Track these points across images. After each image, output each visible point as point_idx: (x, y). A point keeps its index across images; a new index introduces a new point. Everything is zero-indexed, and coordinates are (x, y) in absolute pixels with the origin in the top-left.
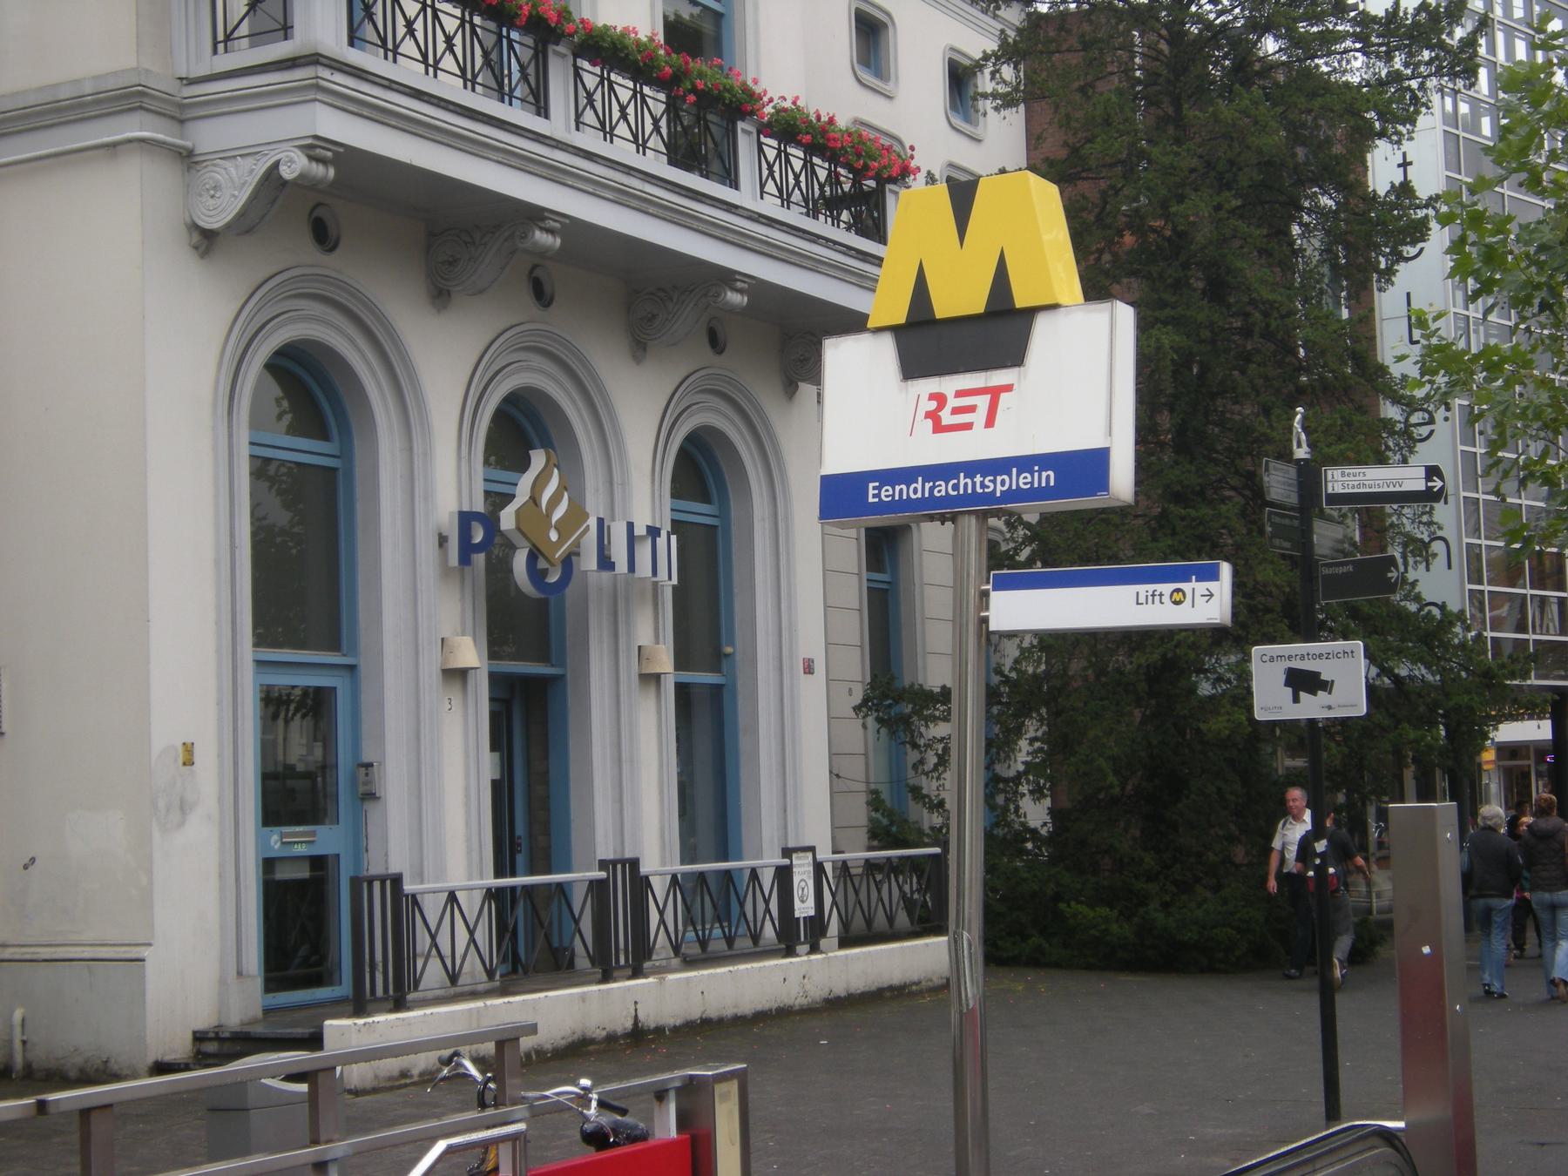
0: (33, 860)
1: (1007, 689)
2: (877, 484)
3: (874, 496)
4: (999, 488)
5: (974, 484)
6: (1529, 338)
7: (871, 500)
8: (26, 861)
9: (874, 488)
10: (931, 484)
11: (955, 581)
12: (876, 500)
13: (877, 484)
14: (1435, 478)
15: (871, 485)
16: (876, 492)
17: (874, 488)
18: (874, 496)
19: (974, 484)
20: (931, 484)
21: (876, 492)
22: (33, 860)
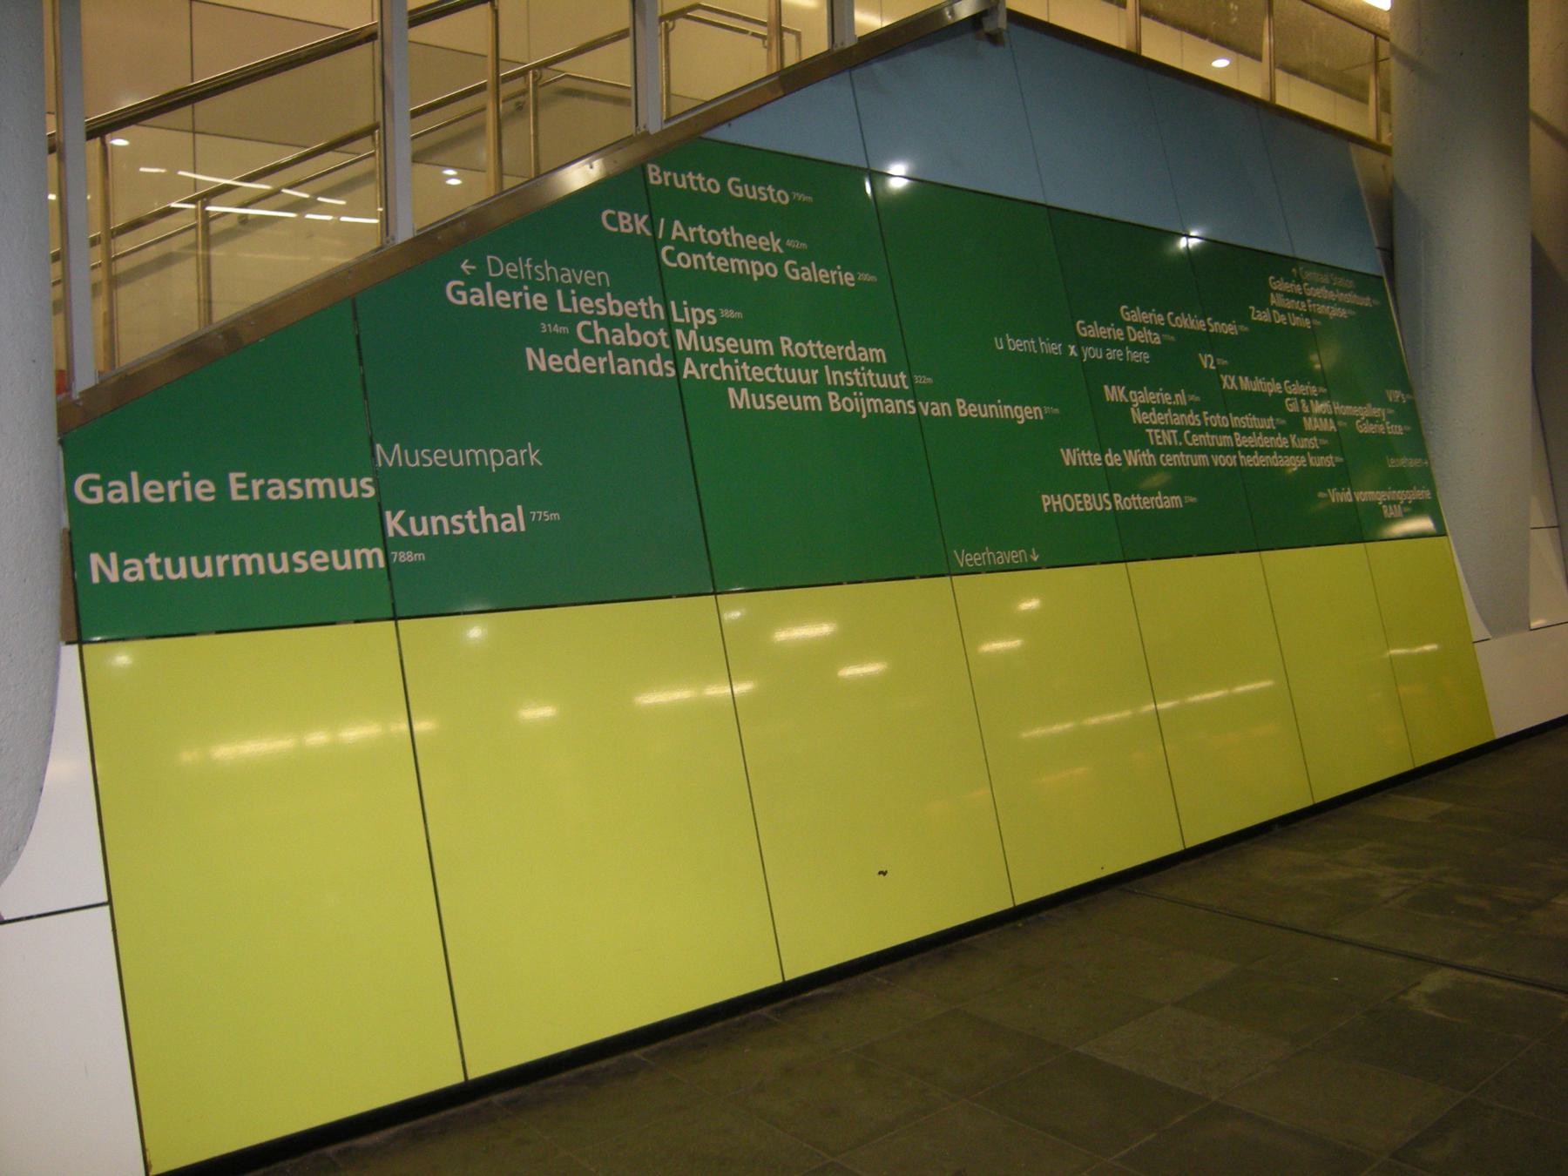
0: (880, 873)
1: (1236, 8)
2: (243, 475)
3: (240, 492)
4: (576, 359)
5: (147, 568)
6: (374, 140)
7: (235, 497)
8: (881, 875)
9: (239, 480)
10: (262, 482)
11: (185, 105)
12: (245, 497)
13: (243, 475)
14: (468, 273)
15: (233, 476)
16: (243, 486)
17: (239, 480)
18: (240, 492)
19: (147, 568)
20: (262, 482)
21: (243, 486)
22: (880, 873)
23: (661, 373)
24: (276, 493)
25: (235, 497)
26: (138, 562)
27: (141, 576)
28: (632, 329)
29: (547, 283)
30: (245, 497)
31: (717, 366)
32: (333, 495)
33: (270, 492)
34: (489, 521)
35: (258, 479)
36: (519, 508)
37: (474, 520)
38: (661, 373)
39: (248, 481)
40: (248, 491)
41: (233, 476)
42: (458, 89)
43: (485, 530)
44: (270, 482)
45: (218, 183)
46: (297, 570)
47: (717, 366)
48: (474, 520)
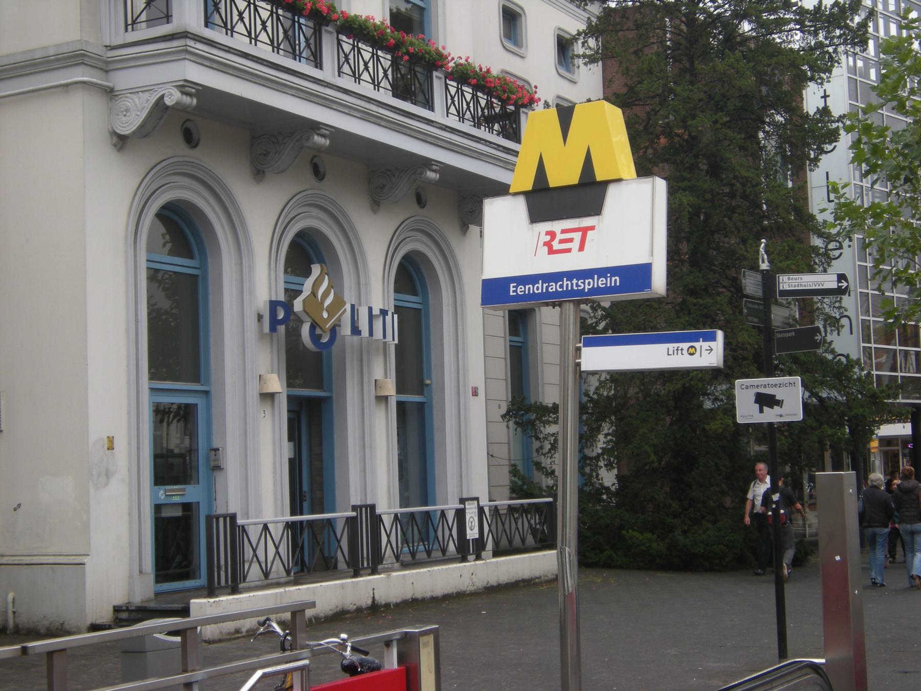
0: (19, 505)
2: (515, 284)
3: (514, 291)
5: (572, 285)
6: (898, 199)
7: (512, 294)
8: (16, 506)
9: (513, 287)
10: (547, 284)
12: (515, 294)
13: (515, 284)
15: (512, 285)
16: (515, 289)
17: (513, 287)
18: (514, 291)
19: (572, 285)
20: (547, 284)
21: (515, 289)
22: (19, 505)
26: (554, 284)
27: (554, 290)
42: (764, 670)
45: (274, 629)
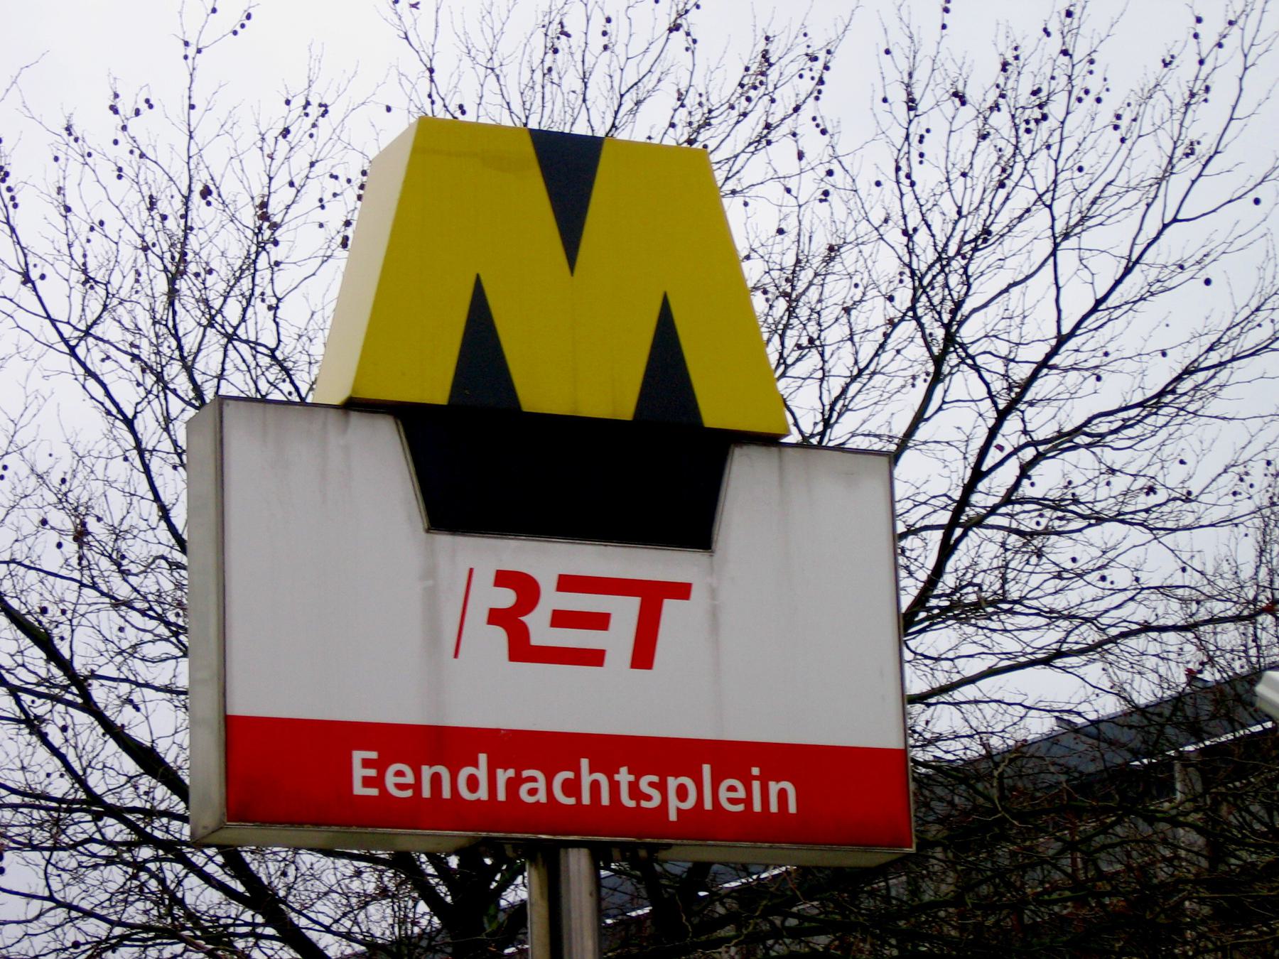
2: (373, 755)
3: (367, 782)
7: (359, 789)
9: (367, 763)
10: (511, 773)
12: (374, 792)
13: (373, 755)
16: (372, 772)
17: (367, 763)
18: (367, 782)
20: (511, 773)
21: (372, 772)
23: (672, 783)
24: (533, 792)
25: (359, 789)
28: (592, 771)
29: (1047, 923)
30: (374, 792)
31: (570, 775)
32: (446, 793)
33: (524, 789)
34: (595, 786)
35: (506, 769)
36: (706, 769)
37: (630, 783)
38: (672, 783)
39: (381, 766)
40: (378, 782)
41: (358, 756)
43: (586, 800)
44: (526, 773)
46: (655, 779)
47: (570, 775)
48: (630, 783)
